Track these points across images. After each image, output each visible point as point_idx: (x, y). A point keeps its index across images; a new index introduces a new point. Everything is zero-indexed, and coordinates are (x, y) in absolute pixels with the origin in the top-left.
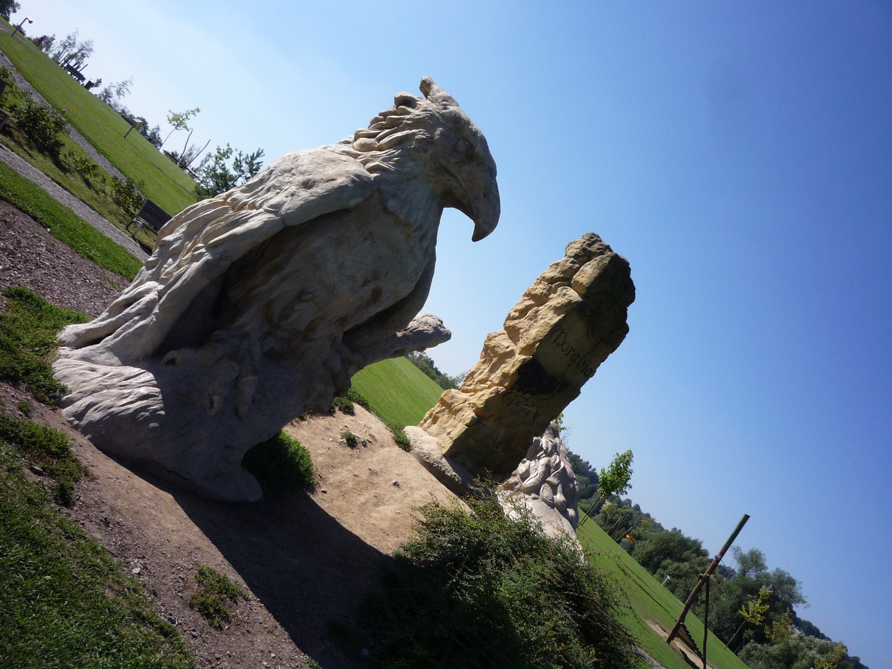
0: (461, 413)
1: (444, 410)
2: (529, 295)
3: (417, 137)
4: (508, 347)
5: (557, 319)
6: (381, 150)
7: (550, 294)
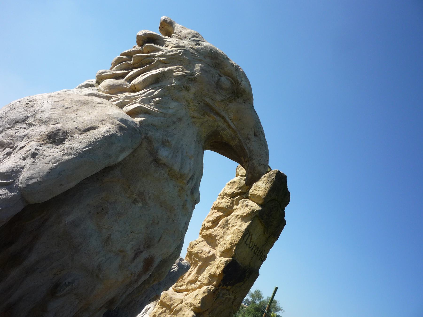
0: (180, 312)
1: (165, 311)
2: (217, 208)
3: (175, 74)
4: (209, 252)
5: (245, 226)
6: (134, 91)
7: (233, 206)
